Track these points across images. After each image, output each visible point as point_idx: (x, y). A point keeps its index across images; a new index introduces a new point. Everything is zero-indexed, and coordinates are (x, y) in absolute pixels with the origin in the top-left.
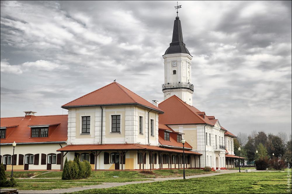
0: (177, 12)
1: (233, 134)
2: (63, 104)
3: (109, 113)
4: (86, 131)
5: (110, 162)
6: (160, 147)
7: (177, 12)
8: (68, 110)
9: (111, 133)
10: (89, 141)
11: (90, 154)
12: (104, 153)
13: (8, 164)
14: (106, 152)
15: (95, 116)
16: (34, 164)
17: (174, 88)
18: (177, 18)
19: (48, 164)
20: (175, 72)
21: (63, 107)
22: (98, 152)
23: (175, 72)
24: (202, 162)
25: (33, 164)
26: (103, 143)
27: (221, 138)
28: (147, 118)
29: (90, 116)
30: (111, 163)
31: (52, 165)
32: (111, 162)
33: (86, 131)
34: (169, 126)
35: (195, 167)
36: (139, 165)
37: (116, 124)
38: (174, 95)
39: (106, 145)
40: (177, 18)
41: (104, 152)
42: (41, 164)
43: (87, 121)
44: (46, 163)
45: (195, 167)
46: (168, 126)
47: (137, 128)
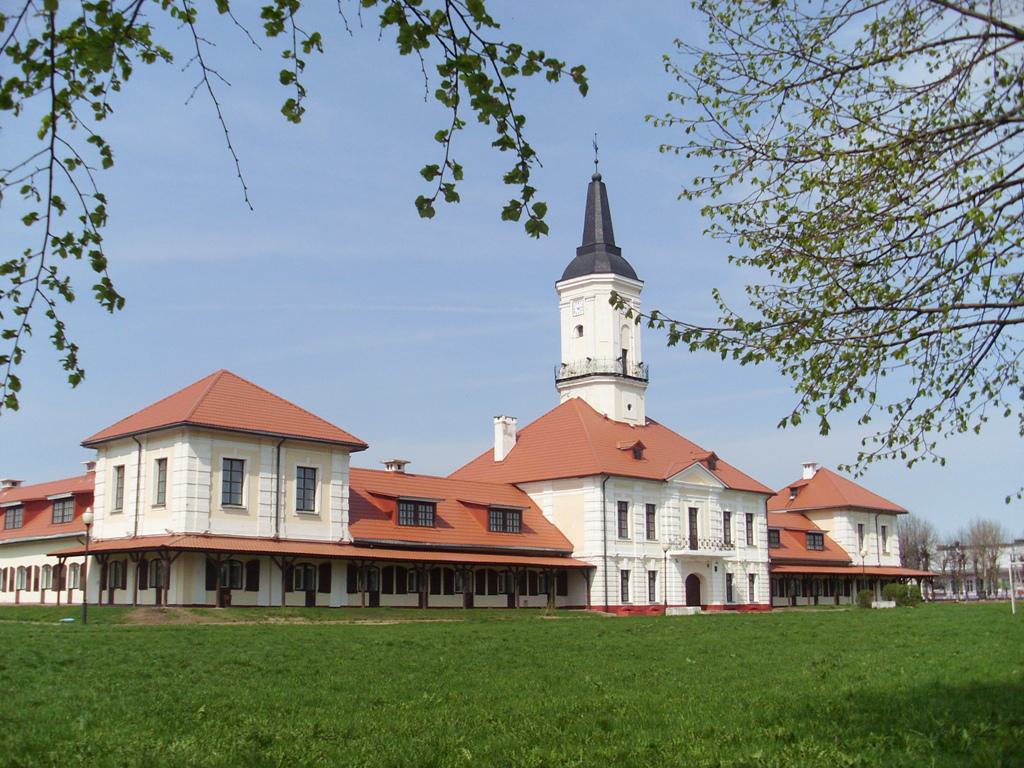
1: (112, 475)
2: (85, 438)
3: (150, 456)
6: (357, 544)
8: (96, 451)
9: (154, 507)
11: (245, 563)
15: (129, 459)
16: (247, 589)
18: (597, 178)
21: (85, 445)
22: (172, 554)
24: (681, 589)
25: (241, 589)
26: (139, 534)
31: (232, 591)
34: (519, 486)
35: (100, 601)
38: (579, 398)
39: (143, 538)
40: (597, 178)
41: (347, 561)
44: (67, 587)
45: (100, 601)
46: (518, 488)
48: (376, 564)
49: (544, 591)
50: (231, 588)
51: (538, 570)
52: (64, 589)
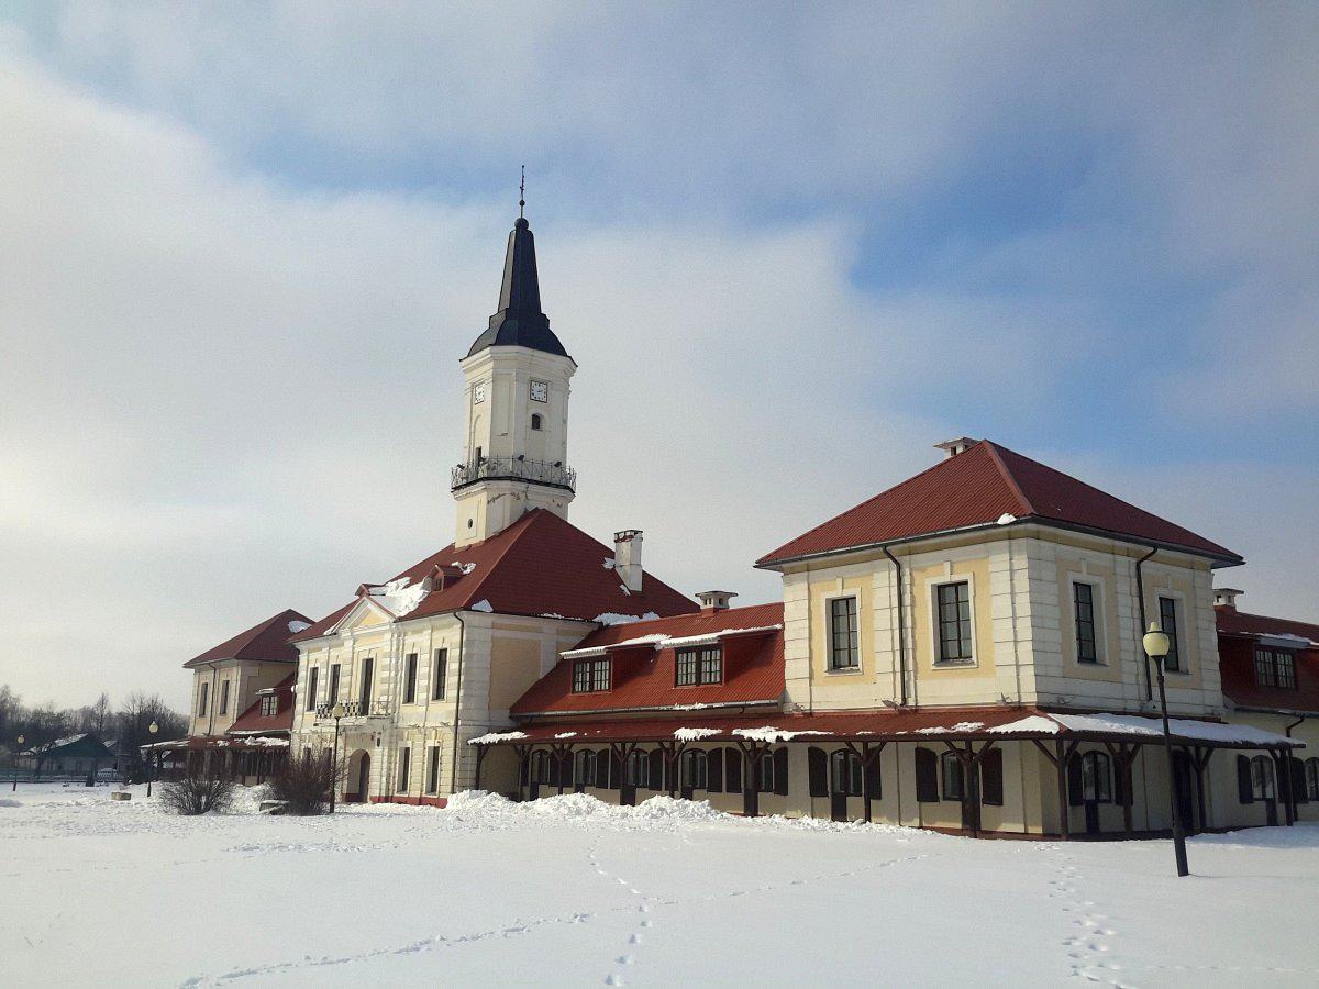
0: (522, 203)
4: (841, 658)
5: (940, 794)
10: (867, 691)
12: (809, 749)
13: (375, 789)
14: (923, 745)
15: (874, 589)
17: (548, 484)
19: (834, 794)
20: (536, 422)
21: (762, 564)
25: (1110, 801)
27: (322, 696)
28: (1126, 587)
29: (966, 583)
30: (945, 798)
32: (949, 794)
33: (841, 658)
36: (1122, 808)
37: (955, 606)
40: (522, 225)
41: (807, 745)
42: (1001, 804)
43: (958, 602)
47: (452, 666)
52: (527, 785)
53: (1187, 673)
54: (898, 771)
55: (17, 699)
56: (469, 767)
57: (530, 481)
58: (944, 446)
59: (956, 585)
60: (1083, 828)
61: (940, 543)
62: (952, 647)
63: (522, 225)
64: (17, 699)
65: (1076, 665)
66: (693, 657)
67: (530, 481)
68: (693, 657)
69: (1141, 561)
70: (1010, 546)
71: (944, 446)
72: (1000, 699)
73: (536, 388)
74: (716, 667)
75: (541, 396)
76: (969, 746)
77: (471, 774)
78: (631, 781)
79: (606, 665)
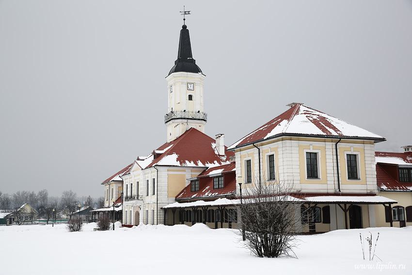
0: (184, 20)
7: (184, 20)
20: (190, 97)
23: (190, 97)
40: (184, 27)
48: (318, 205)
49: (397, 219)
50: (315, 222)
51: (191, 209)
53: (360, 179)
54: (337, 215)
55: (83, 197)
56: (162, 219)
57: (188, 119)
58: (289, 105)
59: (355, 155)
60: (308, 230)
61: (269, 142)
62: (353, 174)
63: (184, 27)
64: (83, 197)
65: (306, 179)
66: (217, 179)
67: (188, 119)
68: (217, 179)
69: (337, 143)
70: (282, 143)
71: (289, 105)
72: (88, 197)
73: (189, 86)
74: (223, 182)
75: (192, 88)
76: (390, 205)
77: (162, 218)
78: (184, 220)
79: (198, 182)
